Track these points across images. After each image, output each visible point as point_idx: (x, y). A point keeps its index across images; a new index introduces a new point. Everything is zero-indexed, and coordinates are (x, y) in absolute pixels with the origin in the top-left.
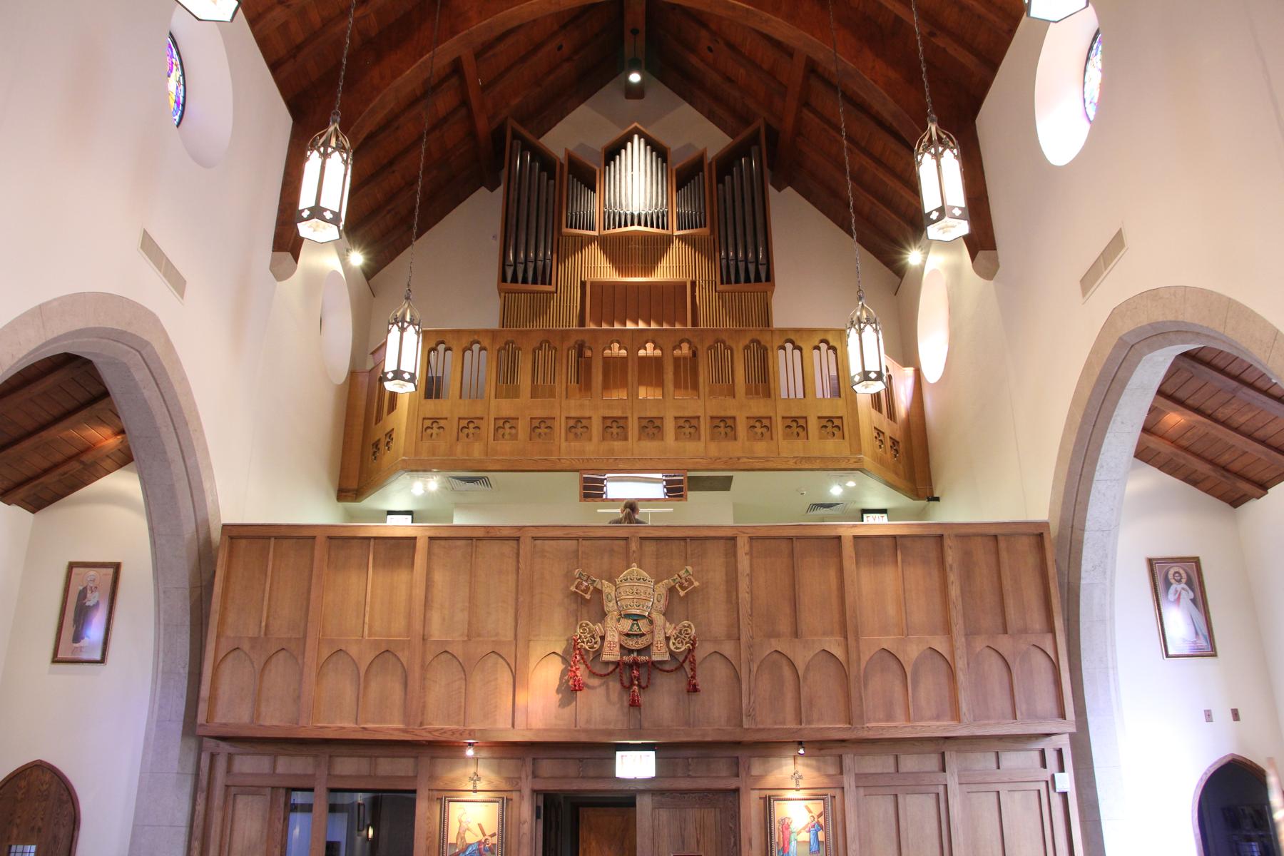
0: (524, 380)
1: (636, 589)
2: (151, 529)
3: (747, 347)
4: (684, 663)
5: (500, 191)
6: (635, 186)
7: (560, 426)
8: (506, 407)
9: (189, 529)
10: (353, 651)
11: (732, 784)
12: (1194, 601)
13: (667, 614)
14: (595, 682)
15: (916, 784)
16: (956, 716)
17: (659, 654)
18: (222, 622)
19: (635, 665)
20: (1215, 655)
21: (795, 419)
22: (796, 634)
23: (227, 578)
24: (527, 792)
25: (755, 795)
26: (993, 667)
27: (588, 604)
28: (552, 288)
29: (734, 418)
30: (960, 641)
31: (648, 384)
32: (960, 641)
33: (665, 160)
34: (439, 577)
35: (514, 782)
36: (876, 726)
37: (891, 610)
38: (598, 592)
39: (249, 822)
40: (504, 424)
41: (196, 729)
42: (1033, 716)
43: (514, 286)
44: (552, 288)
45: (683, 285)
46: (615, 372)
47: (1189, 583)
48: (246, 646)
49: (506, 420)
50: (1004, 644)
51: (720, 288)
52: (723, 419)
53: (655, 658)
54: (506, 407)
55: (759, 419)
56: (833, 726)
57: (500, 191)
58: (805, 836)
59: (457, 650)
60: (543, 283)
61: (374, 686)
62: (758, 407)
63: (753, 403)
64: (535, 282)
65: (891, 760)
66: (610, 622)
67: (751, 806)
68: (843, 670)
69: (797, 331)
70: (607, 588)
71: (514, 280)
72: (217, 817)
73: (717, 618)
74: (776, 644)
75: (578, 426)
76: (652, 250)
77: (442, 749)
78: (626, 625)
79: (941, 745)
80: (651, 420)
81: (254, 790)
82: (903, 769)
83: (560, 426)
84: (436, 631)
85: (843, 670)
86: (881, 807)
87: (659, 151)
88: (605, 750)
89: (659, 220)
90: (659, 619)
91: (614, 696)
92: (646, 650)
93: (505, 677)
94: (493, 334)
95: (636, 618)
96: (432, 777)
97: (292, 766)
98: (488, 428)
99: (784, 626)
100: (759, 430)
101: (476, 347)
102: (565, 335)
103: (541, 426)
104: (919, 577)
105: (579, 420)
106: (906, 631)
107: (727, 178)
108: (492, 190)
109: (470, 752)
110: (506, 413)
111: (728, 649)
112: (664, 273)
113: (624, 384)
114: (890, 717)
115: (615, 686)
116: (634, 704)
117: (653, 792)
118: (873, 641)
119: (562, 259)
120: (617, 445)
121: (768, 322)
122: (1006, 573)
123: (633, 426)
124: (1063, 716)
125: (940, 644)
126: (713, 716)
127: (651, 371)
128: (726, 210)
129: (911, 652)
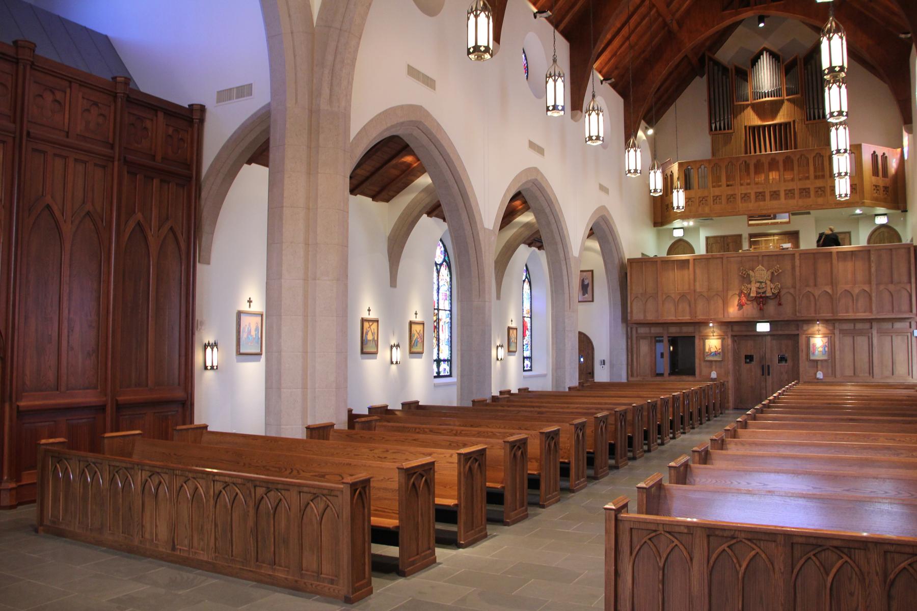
0: (724, 178)
2: (605, 261)
4: (777, 296)
5: (705, 77)
7: (739, 197)
9: (617, 261)
10: (673, 296)
11: (796, 332)
15: (861, 333)
16: (871, 311)
17: (769, 294)
18: (631, 289)
19: (761, 297)
22: (815, 285)
26: (886, 296)
30: (874, 287)
32: (874, 287)
34: (698, 271)
35: (726, 333)
36: (842, 315)
37: (849, 276)
38: (748, 275)
39: (644, 347)
40: (717, 198)
41: (625, 319)
42: (900, 312)
45: (790, 123)
46: (759, 168)
50: (891, 287)
54: (717, 191)
56: (828, 316)
57: (705, 77)
58: (821, 349)
61: (680, 306)
63: (817, 181)
66: (753, 284)
67: (802, 340)
70: (751, 273)
71: (720, 129)
72: (635, 346)
73: (788, 281)
74: (808, 289)
75: (746, 197)
76: (773, 108)
77: (705, 324)
78: (758, 285)
79: (870, 321)
81: (644, 338)
83: (739, 197)
84: (698, 289)
85: (831, 297)
86: (848, 340)
87: (774, 56)
88: (753, 324)
89: (777, 93)
90: (768, 282)
92: (764, 293)
93: (720, 302)
94: (709, 161)
95: (761, 282)
96: (700, 332)
97: (655, 330)
98: (711, 200)
102: (738, 159)
103: (731, 198)
104: (860, 264)
105: (746, 194)
106: (855, 283)
109: (711, 325)
110: (717, 194)
111: (792, 291)
112: (780, 119)
114: (847, 312)
115: (755, 303)
117: (771, 335)
118: (842, 287)
119: (735, 116)
120: (761, 203)
124: (911, 311)
125: (867, 289)
126: (787, 312)
127: (773, 164)
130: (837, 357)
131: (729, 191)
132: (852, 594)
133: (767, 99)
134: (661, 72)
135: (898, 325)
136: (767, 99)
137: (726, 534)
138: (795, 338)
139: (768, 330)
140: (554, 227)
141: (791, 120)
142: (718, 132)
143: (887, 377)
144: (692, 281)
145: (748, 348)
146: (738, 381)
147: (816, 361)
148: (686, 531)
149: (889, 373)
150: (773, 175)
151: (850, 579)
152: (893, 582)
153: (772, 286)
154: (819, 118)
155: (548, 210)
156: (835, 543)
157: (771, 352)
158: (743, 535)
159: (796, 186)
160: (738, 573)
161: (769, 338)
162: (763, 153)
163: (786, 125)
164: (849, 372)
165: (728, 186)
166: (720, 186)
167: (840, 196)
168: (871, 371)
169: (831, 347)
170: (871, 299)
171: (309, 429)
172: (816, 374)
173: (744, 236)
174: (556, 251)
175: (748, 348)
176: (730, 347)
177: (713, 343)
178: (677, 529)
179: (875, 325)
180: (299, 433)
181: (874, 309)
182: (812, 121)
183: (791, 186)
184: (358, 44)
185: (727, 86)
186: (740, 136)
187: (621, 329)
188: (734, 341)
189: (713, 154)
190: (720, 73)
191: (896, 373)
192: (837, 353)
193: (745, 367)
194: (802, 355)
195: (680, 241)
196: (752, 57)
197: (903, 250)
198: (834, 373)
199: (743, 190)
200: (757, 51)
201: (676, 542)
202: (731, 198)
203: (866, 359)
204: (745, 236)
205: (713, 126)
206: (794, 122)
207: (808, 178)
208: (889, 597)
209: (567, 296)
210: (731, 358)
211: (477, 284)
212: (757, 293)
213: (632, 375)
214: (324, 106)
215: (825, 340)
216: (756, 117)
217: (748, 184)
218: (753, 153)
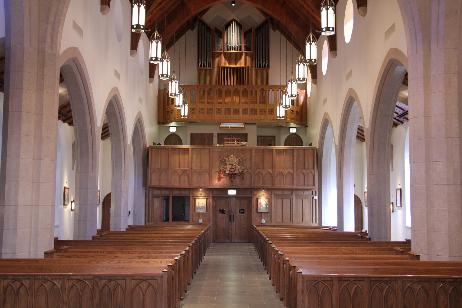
0: (206, 100)
1: (233, 160)
3: (260, 90)
6: (233, 37)
8: (201, 106)
9: (142, 147)
10: (178, 171)
11: (250, 196)
13: (238, 164)
14: (224, 177)
15: (286, 197)
16: (293, 184)
17: (237, 172)
18: (151, 166)
19: (232, 174)
21: (271, 109)
22: (263, 168)
23: (151, 157)
24: (211, 197)
25: (255, 198)
26: (302, 176)
27: (223, 162)
28: (211, 68)
29: (256, 109)
30: (295, 171)
31: (236, 95)
32: (295, 171)
33: (241, 29)
34: (194, 156)
36: (277, 186)
37: (282, 164)
40: (201, 110)
41: (145, 184)
42: (308, 185)
43: (201, 68)
44: (211, 68)
45: (246, 68)
46: (228, 92)
48: (156, 170)
49: (202, 109)
50: (304, 171)
51: (255, 69)
52: (254, 109)
54: (201, 106)
55: (262, 109)
56: (270, 186)
57: (196, 30)
58: (264, 206)
59: (198, 171)
61: (182, 177)
62: (262, 106)
63: (261, 105)
65: (282, 192)
66: (228, 166)
67: (254, 200)
68: (272, 175)
69: (273, 86)
70: (227, 159)
71: (201, 66)
72: (151, 202)
73: (248, 166)
74: (259, 170)
75: (219, 111)
77: (196, 189)
78: (230, 166)
79: (292, 190)
80: (236, 109)
81: (157, 197)
82: (284, 194)
83: (215, 111)
85: (272, 175)
86: (279, 201)
87: (239, 25)
88: (227, 190)
89: (239, 48)
90: (237, 165)
91: (228, 180)
93: (207, 176)
96: (193, 194)
97: (164, 192)
99: (261, 166)
100: (262, 112)
101: (193, 89)
103: (210, 111)
104: (288, 157)
105: (219, 109)
106: (285, 168)
107: (259, 35)
108: (192, 30)
111: (250, 171)
112: (240, 65)
113: (230, 96)
115: (228, 178)
116: (232, 181)
118: (279, 170)
119: (213, 59)
120: (228, 116)
121: (267, 83)
122: (306, 159)
123: (232, 111)
125: (291, 171)
126: (247, 183)
127: (236, 92)
128: (257, 40)
129: (285, 172)
130: (273, 210)
131: (209, 106)
132: (391, 298)
133: (233, 51)
134: (175, 26)
135: (306, 193)
136: (233, 51)
137: (346, 279)
138: (249, 199)
140: (120, 125)
141: (246, 66)
142: (203, 68)
143: (300, 223)
144: (190, 162)
145: (222, 205)
146: (215, 224)
147: (262, 213)
148: (330, 279)
149: (301, 220)
150: (236, 99)
151: (391, 293)
152: (405, 292)
153: (239, 167)
154: (263, 67)
155: (118, 114)
156: (386, 279)
157: (235, 207)
158: (352, 279)
159: (249, 106)
160: (350, 294)
161: (234, 199)
162: (229, 85)
163: (244, 69)
164: (279, 220)
165: (208, 103)
166: (204, 103)
167: (280, 117)
168: (291, 220)
169: (270, 205)
170: (293, 177)
171: (46, 253)
172: (261, 221)
173: (214, 135)
174: (119, 141)
175: (222, 205)
176: (211, 204)
177: (201, 202)
178: (326, 279)
179: (294, 192)
180: (42, 256)
181: (295, 183)
182: (259, 68)
183: (246, 106)
184: (67, 10)
185: (210, 38)
186: (216, 72)
187: (142, 191)
188: (213, 200)
190: (206, 30)
191: (304, 220)
192: (273, 208)
193: (220, 216)
194: (254, 209)
195: (173, 134)
196: (226, 23)
197: (311, 150)
198: (271, 220)
199: (218, 106)
200: (229, 20)
201: (326, 284)
202: (210, 111)
203: (289, 213)
204: (215, 134)
206: (248, 67)
207: (256, 103)
208: (404, 298)
209: (123, 170)
210: (211, 211)
211: (92, 162)
212: (230, 171)
213: (148, 221)
214: (47, 49)
216: (226, 61)
217: (221, 103)
218: (223, 85)
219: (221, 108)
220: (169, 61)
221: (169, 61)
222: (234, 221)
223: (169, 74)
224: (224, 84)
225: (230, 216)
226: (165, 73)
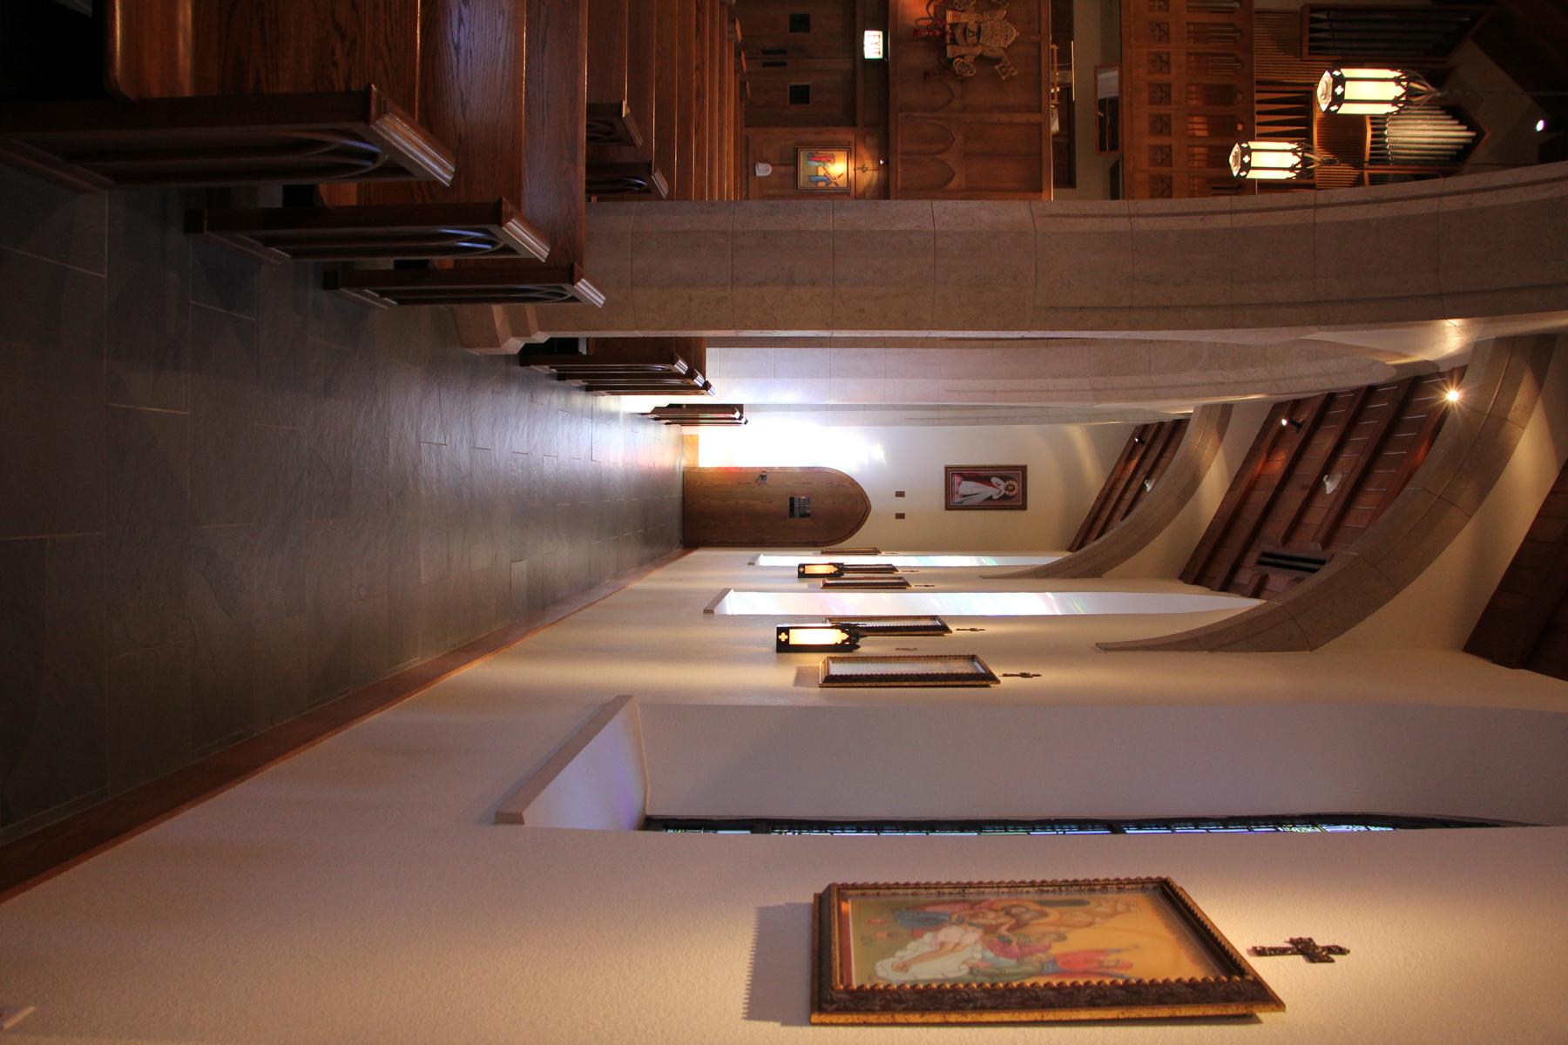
4: (946, 66)
12: (990, 498)
13: (980, 58)
19: (944, 34)
20: (948, 507)
25: (851, 138)
47: (1005, 497)
53: (949, 48)
58: (821, 172)
60: (1310, 48)
64: (1311, 40)
67: (845, 135)
71: (1313, 20)
78: (973, 27)
80: (1168, 125)
90: (978, 51)
92: (954, 42)
95: (978, 33)
103: (1161, 31)
105: (1167, 63)
120: (1145, 96)
133: (1369, 134)
136: (1369, 134)
139: (867, 56)
147: (796, 164)
153: (969, 60)
172: (765, 161)
189: (1258, 12)
194: (809, 134)
202: (1161, 31)
205: (1323, 16)
215: (842, 182)
218: (1258, 97)
219: (1173, 70)
220: (1292, 175)
221: (1292, 175)
222: (765, 65)
223: (1253, 175)
224: (1259, 102)
225: (783, 52)
226: (1257, 159)
